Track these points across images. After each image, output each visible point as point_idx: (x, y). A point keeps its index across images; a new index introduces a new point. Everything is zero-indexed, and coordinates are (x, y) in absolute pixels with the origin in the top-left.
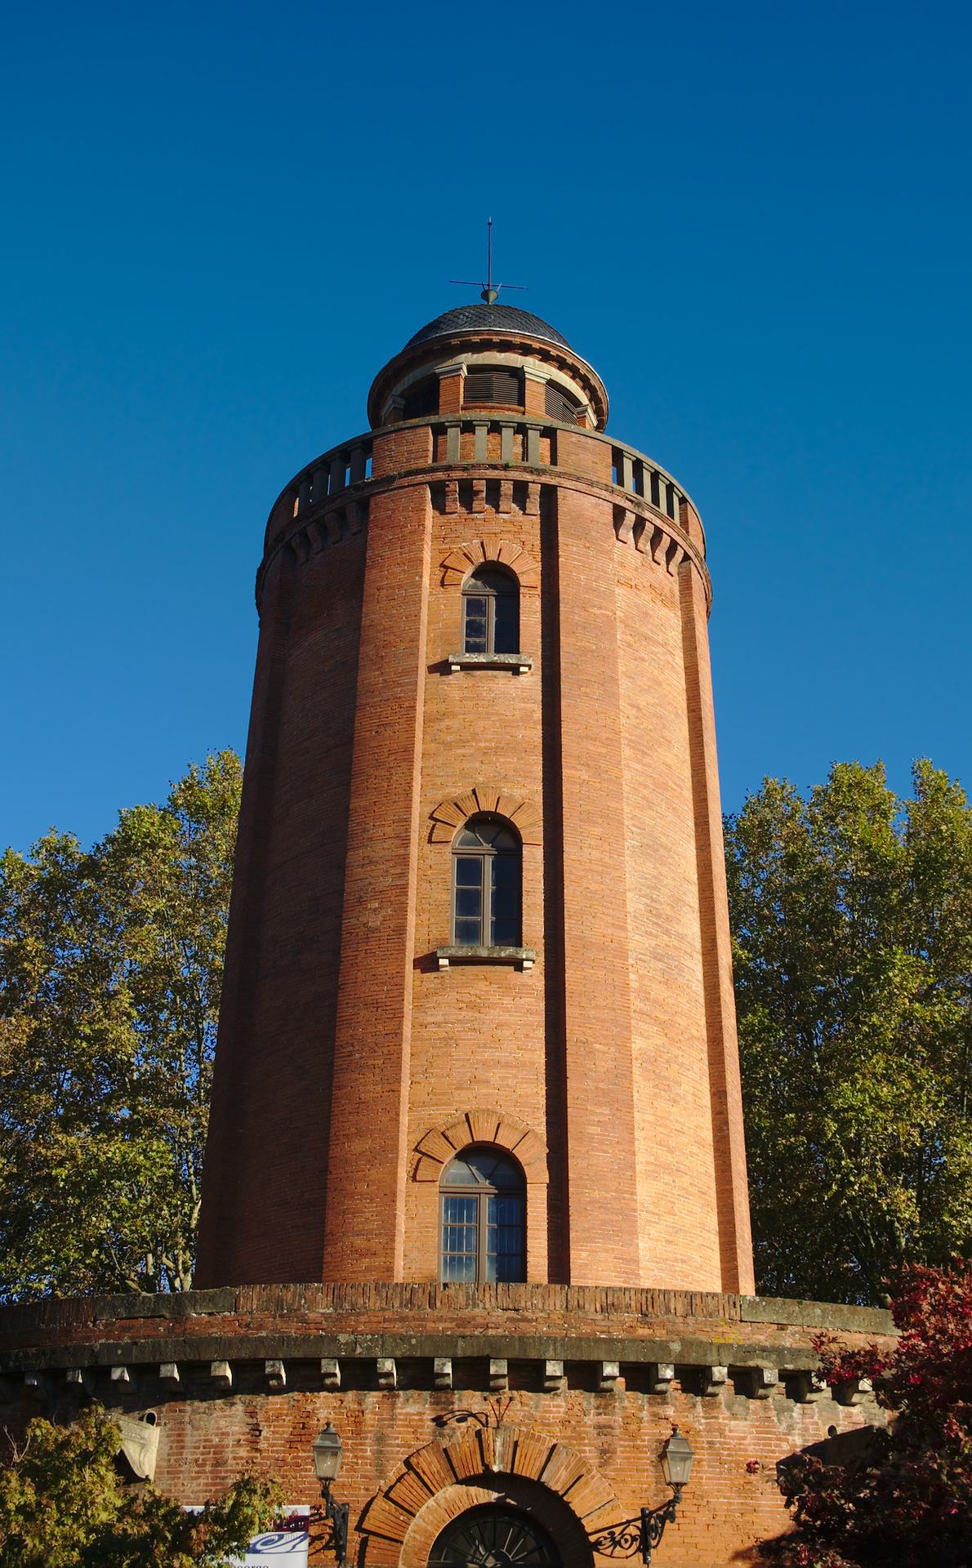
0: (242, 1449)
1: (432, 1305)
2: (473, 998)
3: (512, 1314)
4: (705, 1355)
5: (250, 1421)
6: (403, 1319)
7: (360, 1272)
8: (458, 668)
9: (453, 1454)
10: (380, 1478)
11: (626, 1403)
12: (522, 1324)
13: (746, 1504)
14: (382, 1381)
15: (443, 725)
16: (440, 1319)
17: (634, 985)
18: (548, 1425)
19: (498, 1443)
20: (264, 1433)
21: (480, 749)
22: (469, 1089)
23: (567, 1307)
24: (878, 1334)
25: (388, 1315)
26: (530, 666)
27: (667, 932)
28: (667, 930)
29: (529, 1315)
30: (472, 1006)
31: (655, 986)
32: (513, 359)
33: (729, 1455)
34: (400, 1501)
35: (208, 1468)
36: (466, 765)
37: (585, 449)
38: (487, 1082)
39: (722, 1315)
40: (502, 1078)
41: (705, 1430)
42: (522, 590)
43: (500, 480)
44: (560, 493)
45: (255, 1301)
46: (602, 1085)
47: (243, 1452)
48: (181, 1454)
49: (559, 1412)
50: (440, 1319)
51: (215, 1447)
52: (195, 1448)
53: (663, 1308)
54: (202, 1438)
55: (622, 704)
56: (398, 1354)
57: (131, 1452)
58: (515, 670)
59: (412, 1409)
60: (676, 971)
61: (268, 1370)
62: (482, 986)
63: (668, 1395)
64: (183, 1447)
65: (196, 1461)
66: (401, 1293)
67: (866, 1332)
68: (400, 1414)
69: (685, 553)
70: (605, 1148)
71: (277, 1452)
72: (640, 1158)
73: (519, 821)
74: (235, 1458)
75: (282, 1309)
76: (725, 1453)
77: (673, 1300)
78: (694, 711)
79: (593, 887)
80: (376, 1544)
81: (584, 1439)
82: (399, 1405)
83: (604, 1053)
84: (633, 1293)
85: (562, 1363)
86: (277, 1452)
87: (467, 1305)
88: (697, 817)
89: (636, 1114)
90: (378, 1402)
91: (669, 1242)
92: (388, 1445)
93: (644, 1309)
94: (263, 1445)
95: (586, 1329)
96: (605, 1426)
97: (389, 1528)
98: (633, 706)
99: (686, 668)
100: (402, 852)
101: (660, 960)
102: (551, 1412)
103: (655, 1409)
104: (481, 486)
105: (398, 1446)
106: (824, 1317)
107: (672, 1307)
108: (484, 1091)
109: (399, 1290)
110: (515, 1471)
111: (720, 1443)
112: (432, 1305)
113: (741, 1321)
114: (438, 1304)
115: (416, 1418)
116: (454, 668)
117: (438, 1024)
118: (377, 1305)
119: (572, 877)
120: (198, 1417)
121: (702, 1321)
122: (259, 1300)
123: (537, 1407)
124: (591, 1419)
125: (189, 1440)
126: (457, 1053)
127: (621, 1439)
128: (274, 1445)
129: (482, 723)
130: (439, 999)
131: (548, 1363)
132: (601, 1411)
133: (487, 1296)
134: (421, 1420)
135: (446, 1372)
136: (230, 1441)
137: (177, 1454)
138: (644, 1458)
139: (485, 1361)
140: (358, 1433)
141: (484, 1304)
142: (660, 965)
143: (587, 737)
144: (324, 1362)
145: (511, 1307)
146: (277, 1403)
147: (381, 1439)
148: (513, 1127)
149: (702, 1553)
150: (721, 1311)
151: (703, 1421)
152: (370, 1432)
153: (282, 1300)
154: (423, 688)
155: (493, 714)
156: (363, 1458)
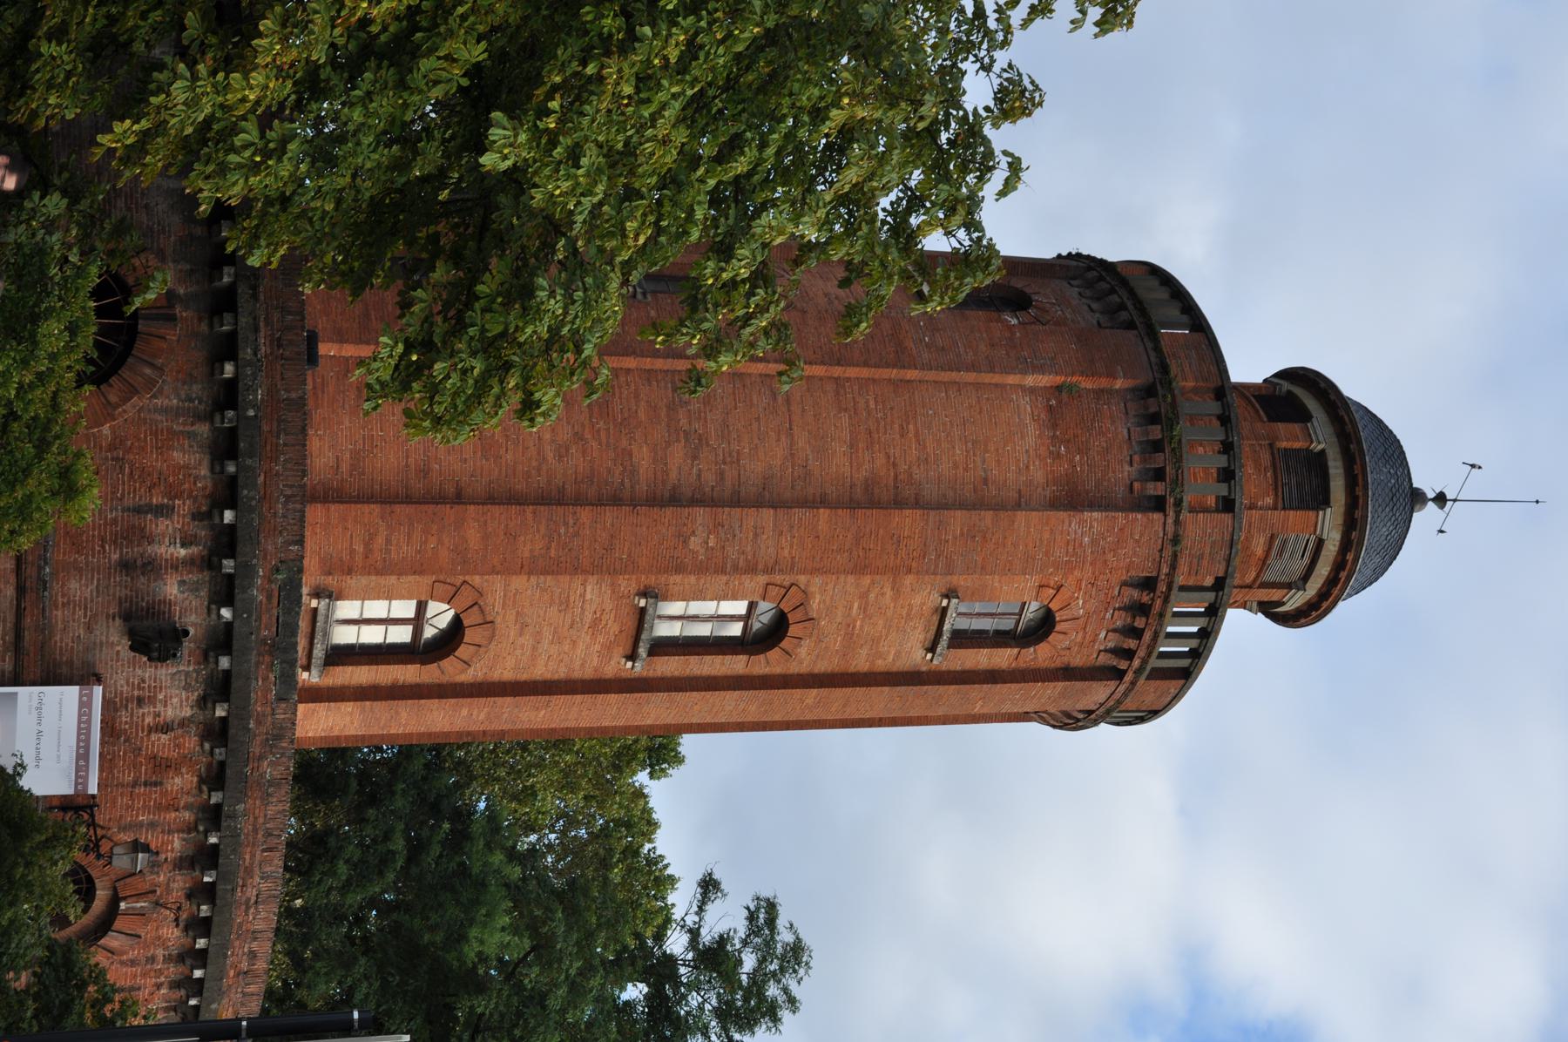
2: (604, 622)
3: (253, 899)
6: (255, 831)
7: (351, 543)
10: (119, 828)
12: (243, 907)
16: (253, 856)
19: (143, 904)
20: (164, 736)
22: (516, 621)
30: (595, 623)
35: (136, 693)
40: (522, 647)
43: (1140, 640)
45: (282, 716)
47: (149, 720)
51: (155, 697)
52: (155, 679)
56: (222, 847)
59: (177, 844)
62: (615, 628)
65: (144, 681)
71: (147, 748)
73: (774, 654)
74: (143, 714)
86: (147, 748)
92: (147, 830)
94: (154, 737)
104: (1140, 623)
108: (512, 633)
112: (264, 850)
117: (583, 595)
120: (183, 678)
126: (553, 611)
128: (153, 746)
129: (881, 622)
140: (159, 808)
154: (993, 381)
155: (889, 631)
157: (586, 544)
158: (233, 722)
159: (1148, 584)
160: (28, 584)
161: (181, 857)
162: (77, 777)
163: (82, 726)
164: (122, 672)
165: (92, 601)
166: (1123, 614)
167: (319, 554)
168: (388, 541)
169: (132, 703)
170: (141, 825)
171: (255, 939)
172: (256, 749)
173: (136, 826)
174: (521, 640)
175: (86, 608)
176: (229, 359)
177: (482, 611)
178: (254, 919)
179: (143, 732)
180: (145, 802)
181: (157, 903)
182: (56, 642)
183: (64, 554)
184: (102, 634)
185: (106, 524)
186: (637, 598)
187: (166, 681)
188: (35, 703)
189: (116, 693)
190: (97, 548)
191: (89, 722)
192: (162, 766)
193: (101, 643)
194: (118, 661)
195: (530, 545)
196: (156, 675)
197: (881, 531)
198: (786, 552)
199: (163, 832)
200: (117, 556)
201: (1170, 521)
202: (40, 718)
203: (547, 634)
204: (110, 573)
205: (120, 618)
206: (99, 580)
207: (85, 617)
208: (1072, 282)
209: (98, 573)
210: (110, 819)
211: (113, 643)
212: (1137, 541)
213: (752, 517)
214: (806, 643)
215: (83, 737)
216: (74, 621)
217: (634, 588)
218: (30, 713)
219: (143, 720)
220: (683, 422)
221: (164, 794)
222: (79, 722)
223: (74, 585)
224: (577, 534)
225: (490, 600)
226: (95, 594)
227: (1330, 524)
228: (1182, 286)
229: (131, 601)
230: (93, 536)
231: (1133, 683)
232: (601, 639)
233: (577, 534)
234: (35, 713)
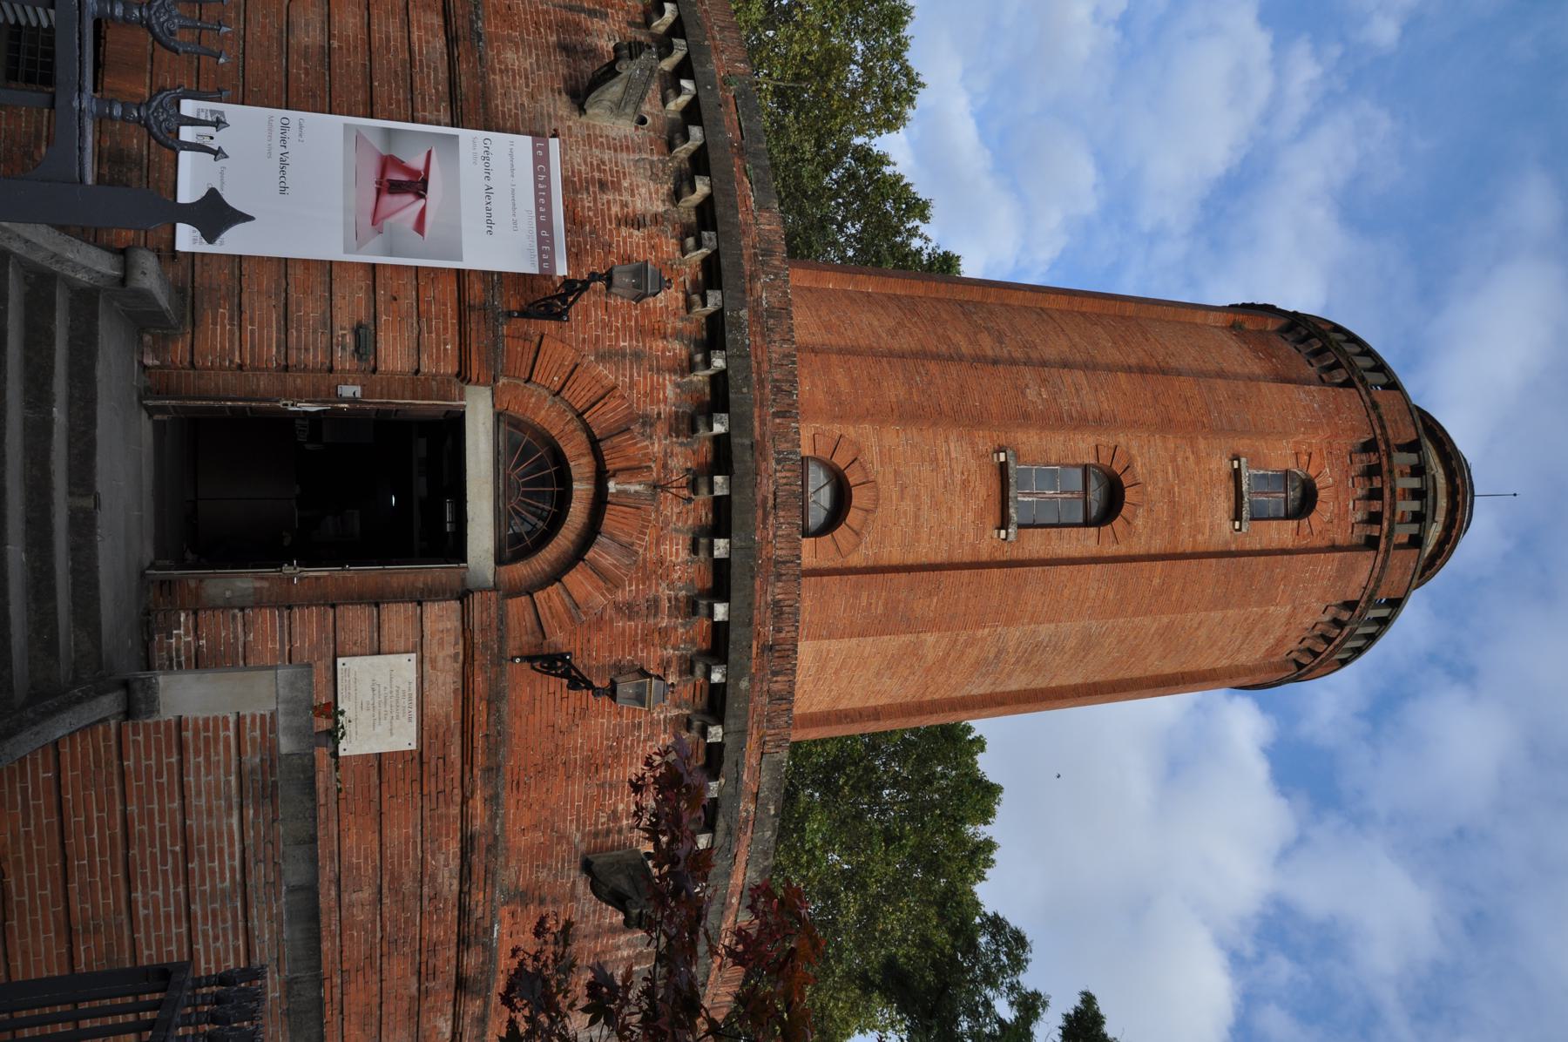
0: (618, 209)
1: (775, 415)
2: (972, 484)
3: (770, 503)
4: (735, 716)
5: (648, 219)
8: (1236, 466)
11: (681, 630)
12: (760, 512)
13: (575, 768)
14: (699, 357)
15: (1189, 453)
16: (763, 423)
17: (980, 633)
18: (658, 544)
19: (638, 488)
21: (1173, 488)
22: (896, 484)
23: (780, 562)
24: (741, 897)
25: (765, 366)
26: (1240, 530)
27: (1017, 662)
28: (1018, 662)
29: (771, 519)
30: (965, 484)
31: (976, 652)
33: (626, 746)
34: (574, 377)
35: (596, 175)
36: (1159, 475)
37: (1404, 574)
38: (902, 499)
39: (770, 732)
40: (905, 513)
41: (653, 718)
44: (1372, 554)
45: (768, 227)
46: (902, 605)
47: (615, 209)
48: (609, 148)
49: (671, 556)
50: (763, 423)
51: (619, 182)
52: (616, 163)
53: (778, 668)
54: (627, 170)
55: (1203, 614)
56: (730, 372)
57: (614, 88)
59: (670, 392)
60: (984, 670)
61: (705, 234)
63: (690, 677)
64: (616, 150)
65: (604, 163)
66: (787, 381)
67: (743, 885)
68: (664, 379)
69: (1304, 666)
70: (848, 610)
71: (618, 245)
72: (834, 645)
75: (762, 256)
76: (629, 743)
77: (786, 679)
78: (1183, 678)
79: (1066, 592)
80: (527, 350)
81: (644, 584)
82: (673, 378)
83: (929, 606)
84: (793, 634)
85: (727, 556)
86: (618, 245)
87: (779, 453)
88: (1042, 691)
89: (871, 639)
90: (675, 354)
92: (631, 363)
93: (777, 647)
94: (624, 231)
96: (657, 607)
97: (544, 365)
98: (1200, 624)
99: (1215, 670)
101: (996, 656)
102: (671, 548)
103: (674, 663)
104: (1377, 483)
105: (631, 376)
107: (779, 679)
109: (791, 378)
110: (609, 506)
111: (640, 736)
112: (775, 415)
113: (762, 753)
114: (778, 421)
115: (661, 396)
116: (1236, 463)
117: (948, 453)
118: (774, 355)
119: (1075, 572)
121: (764, 711)
122: (769, 231)
123: (676, 530)
124: (664, 592)
126: (926, 468)
127: (643, 625)
128: (625, 243)
130: (969, 454)
131: (727, 540)
132: (673, 603)
133: (788, 474)
134: (659, 401)
135: (715, 425)
136: (626, 197)
137: (608, 144)
138: (623, 650)
141: (780, 471)
142: (991, 656)
143: (1185, 583)
144: (718, 294)
145: (778, 500)
146: (668, 247)
147: (637, 356)
149: (524, 720)
150: (773, 732)
151: (662, 716)
152: (644, 345)
153: (770, 256)
156: (617, 337)
159: (1369, 447)
160: (460, 32)
161: (676, 413)
162: (541, 252)
163: (540, 186)
164: (578, 149)
165: (533, 73)
169: (594, 185)
170: (622, 354)
172: (747, 267)
173: (616, 354)
175: (527, 78)
178: (775, 536)
179: (611, 223)
180: (624, 321)
182: (497, 106)
183: (496, 27)
184: (548, 106)
186: (995, 455)
187: (629, 167)
188: (481, 151)
189: (573, 172)
190: (532, 29)
191: (547, 182)
193: (549, 116)
194: (570, 136)
196: (616, 158)
199: (651, 369)
200: (554, 38)
202: (488, 171)
203: (925, 499)
204: (549, 52)
205: (567, 94)
206: (537, 55)
207: (527, 86)
209: (536, 49)
210: (584, 339)
211: (562, 116)
213: (1069, 377)
214: (1140, 511)
215: (542, 177)
216: (515, 88)
217: (990, 446)
218: (475, 163)
219: (609, 209)
222: (536, 182)
223: (510, 55)
224: (930, 383)
226: (535, 66)
229: (577, 81)
230: (526, 19)
232: (973, 505)
233: (930, 383)
234: (481, 163)
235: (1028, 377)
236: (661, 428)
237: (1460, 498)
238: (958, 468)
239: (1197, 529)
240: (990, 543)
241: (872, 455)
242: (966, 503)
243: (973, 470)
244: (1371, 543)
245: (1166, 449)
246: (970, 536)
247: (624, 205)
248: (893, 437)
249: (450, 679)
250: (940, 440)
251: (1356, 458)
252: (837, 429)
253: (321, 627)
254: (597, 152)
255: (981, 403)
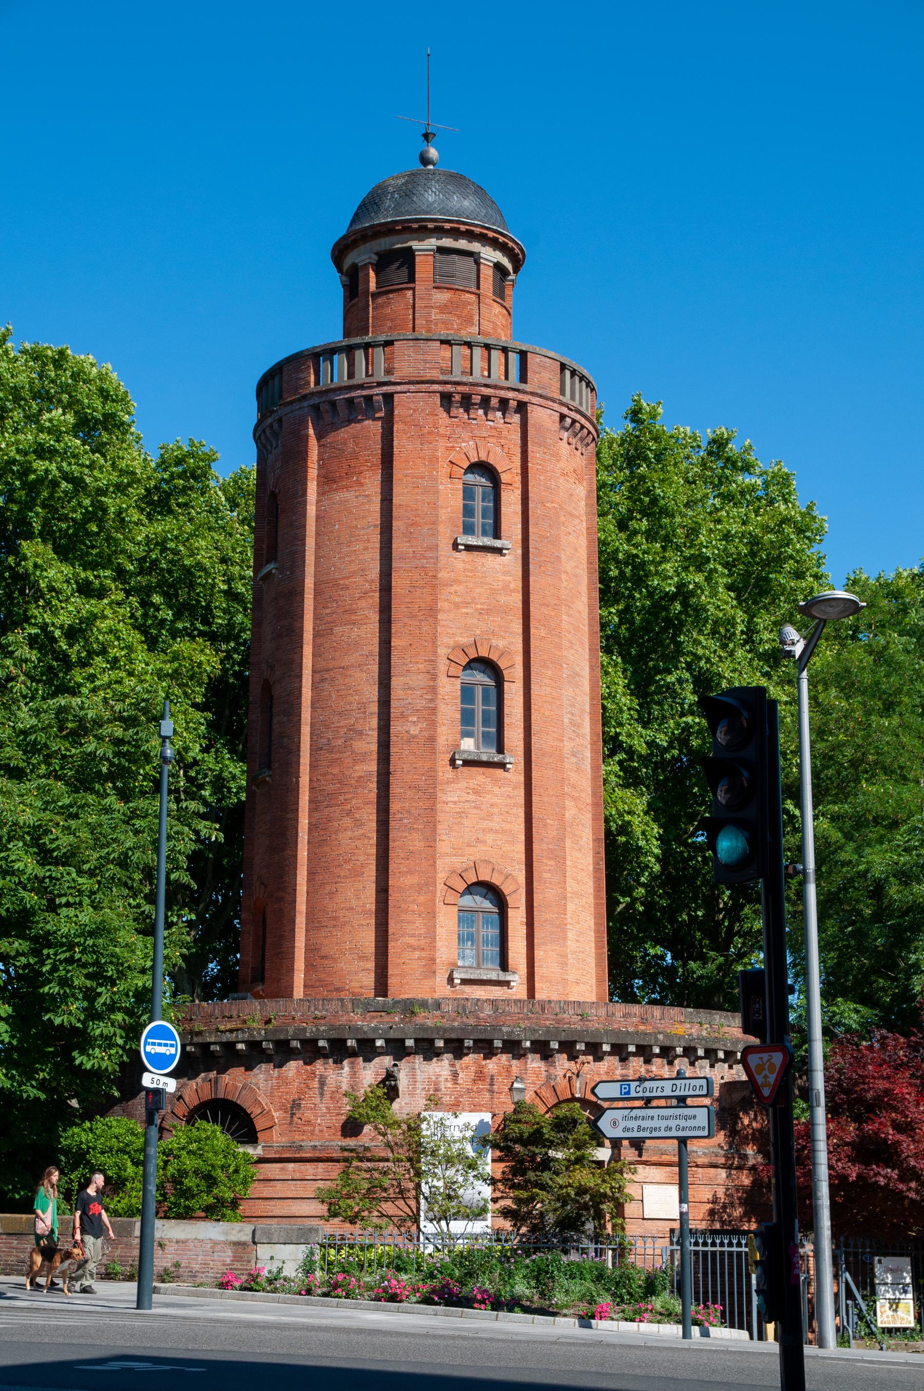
2: (476, 787)
6: (529, 1019)
9: (556, 1088)
30: (477, 793)
32: (475, 247)
36: (469, 621)
42: (503, 486)
46: (551, 847)
47: (449, 1085)
50: (547, 1019)
58: (499, 551)
59: (535, 1065)
62: (481, 778)
79: (547, 713)
91: (577, 941)
94: (460, 1081)
95: (616, 1026)
100: (432, 684)
104: (476, 399)
106: (720, 1017)
108: (484, 848)
117: (455, 803)
125: (419, 1077)
126: (466, 822)
129: (477, 590)
139: (574, 1043)
148: (501, 872)
157: (414, 804)
158: (447, 1036)
159: (446, 399)
166: (471, 411)
167: (421, 980)
168: (412, 936)
171: (613, 1014)
174: (489, 842)
176: (235, 1046)
177: (466, 870)
181: (578, 1076)
185: (329, 1113)
192: (480, 1075)
195: (416, 842)
197: (407, 600)
198: (421, 666)
201: (399, 388)
203: (485, 824)
208: (274, 445)
212: (414, 410)
214: (494, 642)
220: (340, 742)
221: (500, 1074)
224: (408, 812)
225: (458, 866)
227: (424, 246)
228: (275, 365)
231: (532, 394)
233: (408, 812)
235: (399, 728)
236: (552, 1070)
237: (463, 228)
238: (465, 797)
239: (506, 588)
240: (515, 774)
241: (459, 862)
242: (488, 793)
243: (467, 785)
244: (522, 408)
245: (450, 611)
246: (507, 789)
247: (446, 1080)
248: (444, 845)
249: (652, 1171)
250: (447, 808)
251: (454, 411)
252: (440, 887)
253: (632, 1224)
254: (418, 1091)
255: (423, 775)
